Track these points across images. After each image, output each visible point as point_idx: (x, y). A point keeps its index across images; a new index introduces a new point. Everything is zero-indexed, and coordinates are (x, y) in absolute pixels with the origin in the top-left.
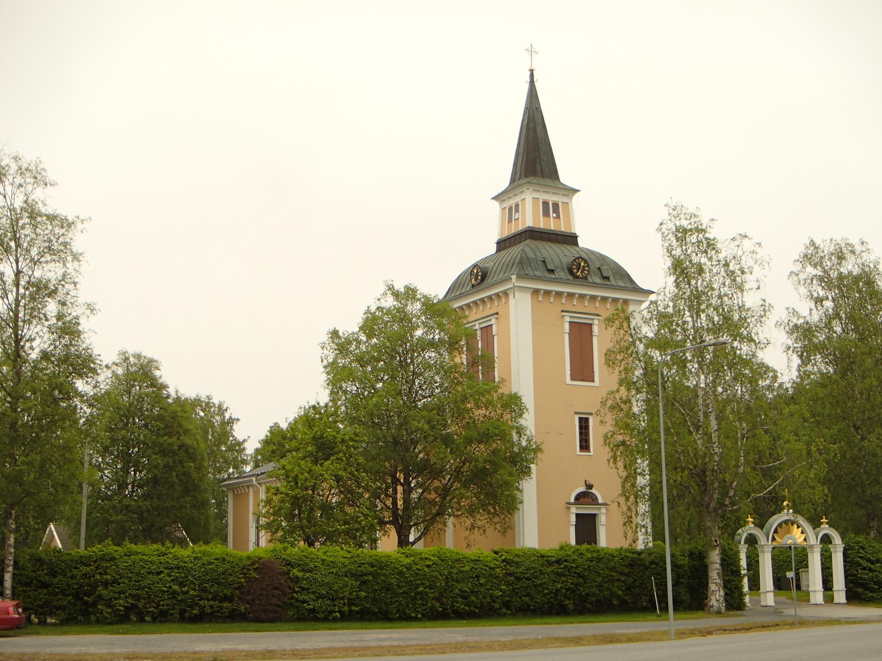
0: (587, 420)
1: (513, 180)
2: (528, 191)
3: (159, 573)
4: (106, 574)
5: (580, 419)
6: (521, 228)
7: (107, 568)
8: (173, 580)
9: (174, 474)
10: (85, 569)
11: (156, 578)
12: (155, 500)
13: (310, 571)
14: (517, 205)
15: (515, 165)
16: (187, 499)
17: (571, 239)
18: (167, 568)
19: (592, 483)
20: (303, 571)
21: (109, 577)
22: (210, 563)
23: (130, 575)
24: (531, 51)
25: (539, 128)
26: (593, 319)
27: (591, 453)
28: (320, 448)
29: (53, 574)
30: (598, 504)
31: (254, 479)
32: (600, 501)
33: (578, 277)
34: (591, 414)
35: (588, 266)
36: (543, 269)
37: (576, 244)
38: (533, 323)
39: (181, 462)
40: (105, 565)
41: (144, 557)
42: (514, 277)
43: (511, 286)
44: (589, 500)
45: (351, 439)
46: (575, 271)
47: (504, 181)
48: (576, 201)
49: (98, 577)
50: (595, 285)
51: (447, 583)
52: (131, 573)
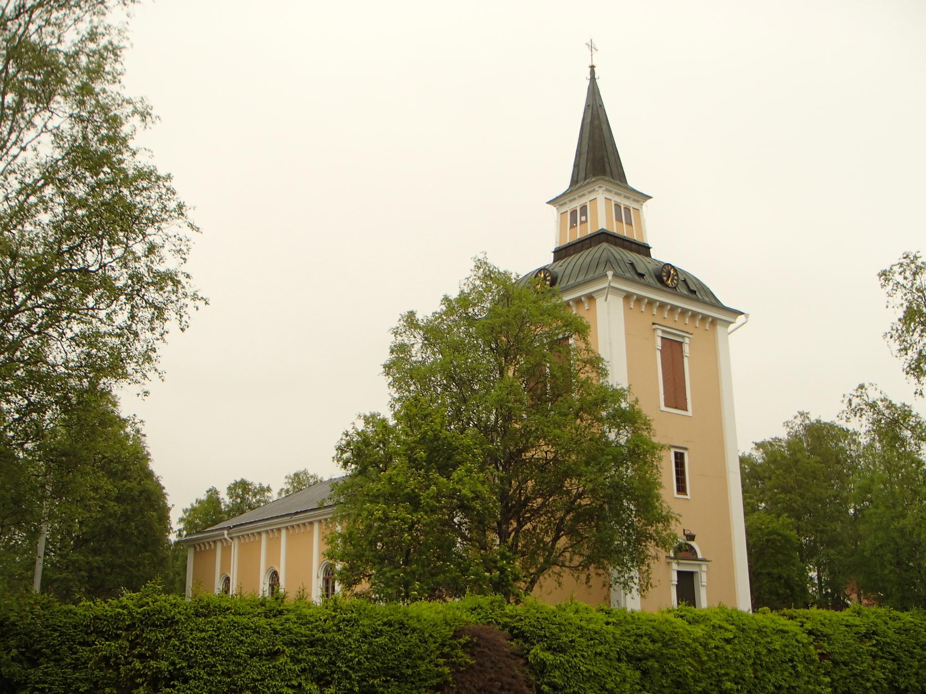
0: (682, 454)
1: (574, 181)
2: (601, 191)
3: (274, 655)
4: (155, 656)
5: (676, 454)
6: (590, 230)
7: (157, 643)
8: (303, 671)
9: (133, 524)
10: (107, 647)
11: (265, 666)
12: (108, 555)
13: (563, 651)
14: (584, 209)
15: (576, 165)
16: (147, 554)
17: (644, 250)
18: (290, 644)
19: (693, 532)
20: (549, 649)
21: (164, 665)
22: (378, 633)
23: (211, 660)
24: (591, 47)
25: (604, 127)
26: (683, 337)
27: (688, 497)
28: (433, 452)
29: (31, 658)
30: (697, 559)
31: (226, 532)
32: (700, 556)
33: (667, 286)
34: (686, 449)
35: (677, 275)
36: (633, 272)
37: (649, 255)
38: (627, 334)
39: (141, 511)
40: (152, 636)
41: (237, 618)
42: (610, 274)
43: (606, 285)
44: (688, 554)
45: (99, 569)
46: (665, 278)
47: (564, 184)
48: (647, 208)
49: (138, 665)
50: (682, 296)
51: (755, 671)
52: (213, 654)
